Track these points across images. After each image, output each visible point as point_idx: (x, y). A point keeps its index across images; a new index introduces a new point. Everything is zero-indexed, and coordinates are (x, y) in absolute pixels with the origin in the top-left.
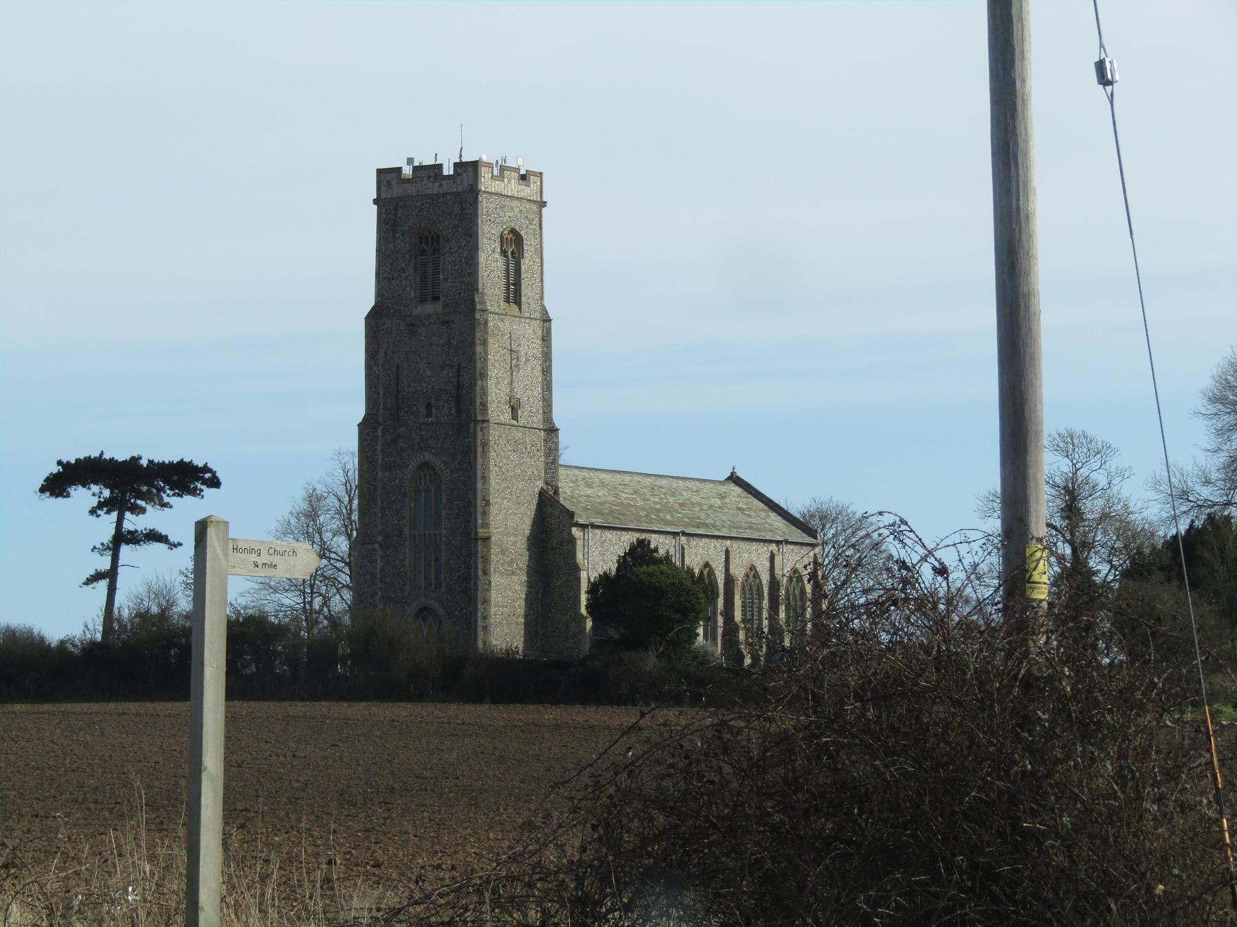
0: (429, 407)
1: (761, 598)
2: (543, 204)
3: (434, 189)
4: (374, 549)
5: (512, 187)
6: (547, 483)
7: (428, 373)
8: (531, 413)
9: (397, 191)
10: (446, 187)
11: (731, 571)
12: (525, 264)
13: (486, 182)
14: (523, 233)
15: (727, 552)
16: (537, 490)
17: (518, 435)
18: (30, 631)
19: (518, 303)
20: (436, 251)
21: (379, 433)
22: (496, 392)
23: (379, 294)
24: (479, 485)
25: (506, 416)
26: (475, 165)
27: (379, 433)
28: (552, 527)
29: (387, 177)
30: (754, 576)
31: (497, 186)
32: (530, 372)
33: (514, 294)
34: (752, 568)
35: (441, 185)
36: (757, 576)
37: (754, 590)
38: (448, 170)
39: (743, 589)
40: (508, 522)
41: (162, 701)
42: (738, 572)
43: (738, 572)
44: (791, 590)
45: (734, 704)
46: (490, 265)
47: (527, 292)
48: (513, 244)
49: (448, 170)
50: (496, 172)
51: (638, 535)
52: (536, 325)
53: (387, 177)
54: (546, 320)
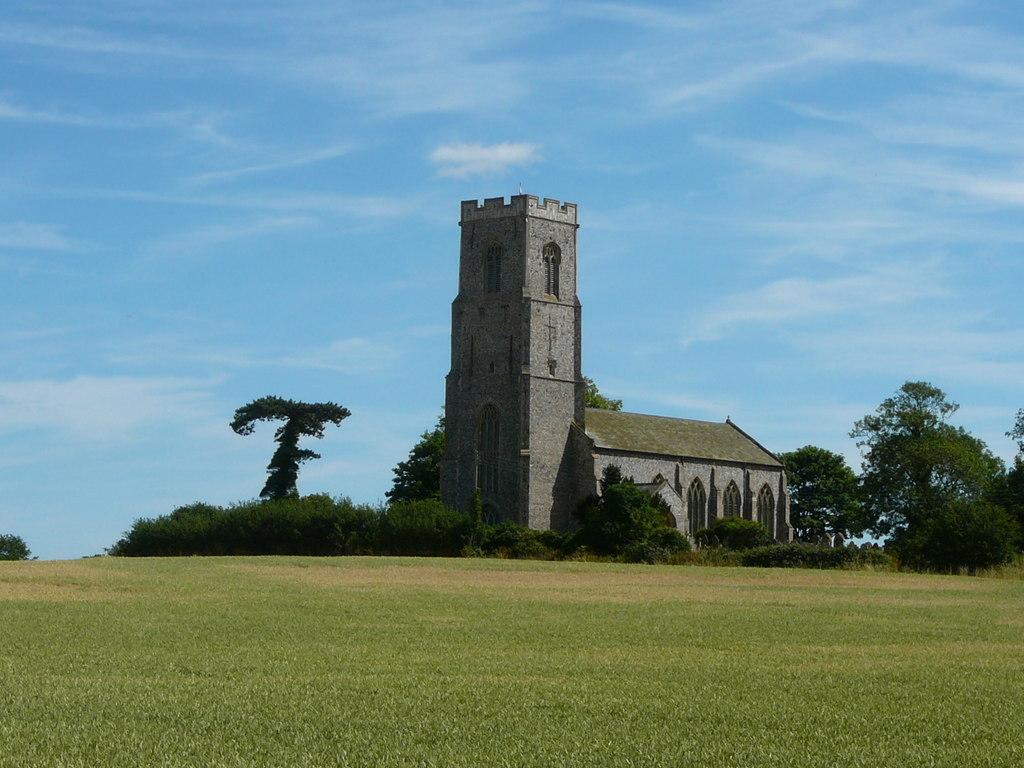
0: (492, 365)
1: (739, 504)
2: (578, 226)
3: (498, 215)
4: (455, 464)
5: (552, 213)
6: (577, 421)
7: (492, 342)
8: (565, 370)
9: (475, 216)
10: (506, 213)
11: (680, 481)
12: (563, 266)
13: (533, 210)
14: (561, 246)
15: (713, 470)
16: (568, 425)
17: (554, 385)
18: (200, 510)
19: (557, 294)
20: (498, 258)
21: (459, 384)
22: (537, 355)
23: (462, 288)
24: (522, 419)
25: (545, 373)
26: (524, 198)
27: (459, 384)
28: (577, 452)
29: (468, 206)
30: (767, 493)
31: (543, 213)
32: (564, 343)
33: (553, 287)
34: (732, 482)
35: (502, 212)
36: (736, 488)
37: (698, 495)
38: (507, 202)
39: (725, 499)
40: (546, 445)
41: (240, 554)
42: (721, 484)
43: (721, 484)
44: (762, 498)
45: (916, 608)
46: (535, 267)
47: (563, 286)
48: (553, 254)
49: (507, 202)
50: (541, 203)
51: (785, 483)
52: (571, 311)
53: (468, 206)
54: (577, 308)
